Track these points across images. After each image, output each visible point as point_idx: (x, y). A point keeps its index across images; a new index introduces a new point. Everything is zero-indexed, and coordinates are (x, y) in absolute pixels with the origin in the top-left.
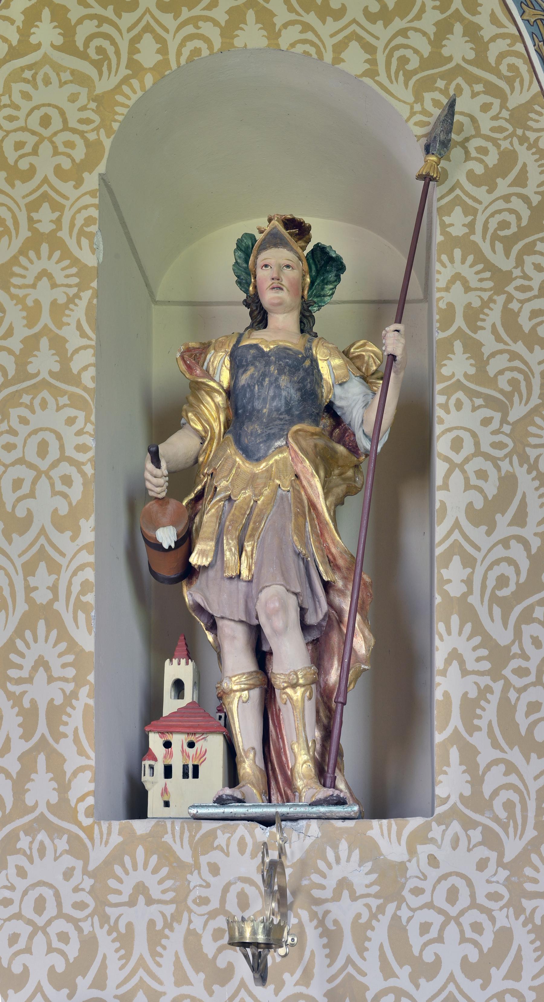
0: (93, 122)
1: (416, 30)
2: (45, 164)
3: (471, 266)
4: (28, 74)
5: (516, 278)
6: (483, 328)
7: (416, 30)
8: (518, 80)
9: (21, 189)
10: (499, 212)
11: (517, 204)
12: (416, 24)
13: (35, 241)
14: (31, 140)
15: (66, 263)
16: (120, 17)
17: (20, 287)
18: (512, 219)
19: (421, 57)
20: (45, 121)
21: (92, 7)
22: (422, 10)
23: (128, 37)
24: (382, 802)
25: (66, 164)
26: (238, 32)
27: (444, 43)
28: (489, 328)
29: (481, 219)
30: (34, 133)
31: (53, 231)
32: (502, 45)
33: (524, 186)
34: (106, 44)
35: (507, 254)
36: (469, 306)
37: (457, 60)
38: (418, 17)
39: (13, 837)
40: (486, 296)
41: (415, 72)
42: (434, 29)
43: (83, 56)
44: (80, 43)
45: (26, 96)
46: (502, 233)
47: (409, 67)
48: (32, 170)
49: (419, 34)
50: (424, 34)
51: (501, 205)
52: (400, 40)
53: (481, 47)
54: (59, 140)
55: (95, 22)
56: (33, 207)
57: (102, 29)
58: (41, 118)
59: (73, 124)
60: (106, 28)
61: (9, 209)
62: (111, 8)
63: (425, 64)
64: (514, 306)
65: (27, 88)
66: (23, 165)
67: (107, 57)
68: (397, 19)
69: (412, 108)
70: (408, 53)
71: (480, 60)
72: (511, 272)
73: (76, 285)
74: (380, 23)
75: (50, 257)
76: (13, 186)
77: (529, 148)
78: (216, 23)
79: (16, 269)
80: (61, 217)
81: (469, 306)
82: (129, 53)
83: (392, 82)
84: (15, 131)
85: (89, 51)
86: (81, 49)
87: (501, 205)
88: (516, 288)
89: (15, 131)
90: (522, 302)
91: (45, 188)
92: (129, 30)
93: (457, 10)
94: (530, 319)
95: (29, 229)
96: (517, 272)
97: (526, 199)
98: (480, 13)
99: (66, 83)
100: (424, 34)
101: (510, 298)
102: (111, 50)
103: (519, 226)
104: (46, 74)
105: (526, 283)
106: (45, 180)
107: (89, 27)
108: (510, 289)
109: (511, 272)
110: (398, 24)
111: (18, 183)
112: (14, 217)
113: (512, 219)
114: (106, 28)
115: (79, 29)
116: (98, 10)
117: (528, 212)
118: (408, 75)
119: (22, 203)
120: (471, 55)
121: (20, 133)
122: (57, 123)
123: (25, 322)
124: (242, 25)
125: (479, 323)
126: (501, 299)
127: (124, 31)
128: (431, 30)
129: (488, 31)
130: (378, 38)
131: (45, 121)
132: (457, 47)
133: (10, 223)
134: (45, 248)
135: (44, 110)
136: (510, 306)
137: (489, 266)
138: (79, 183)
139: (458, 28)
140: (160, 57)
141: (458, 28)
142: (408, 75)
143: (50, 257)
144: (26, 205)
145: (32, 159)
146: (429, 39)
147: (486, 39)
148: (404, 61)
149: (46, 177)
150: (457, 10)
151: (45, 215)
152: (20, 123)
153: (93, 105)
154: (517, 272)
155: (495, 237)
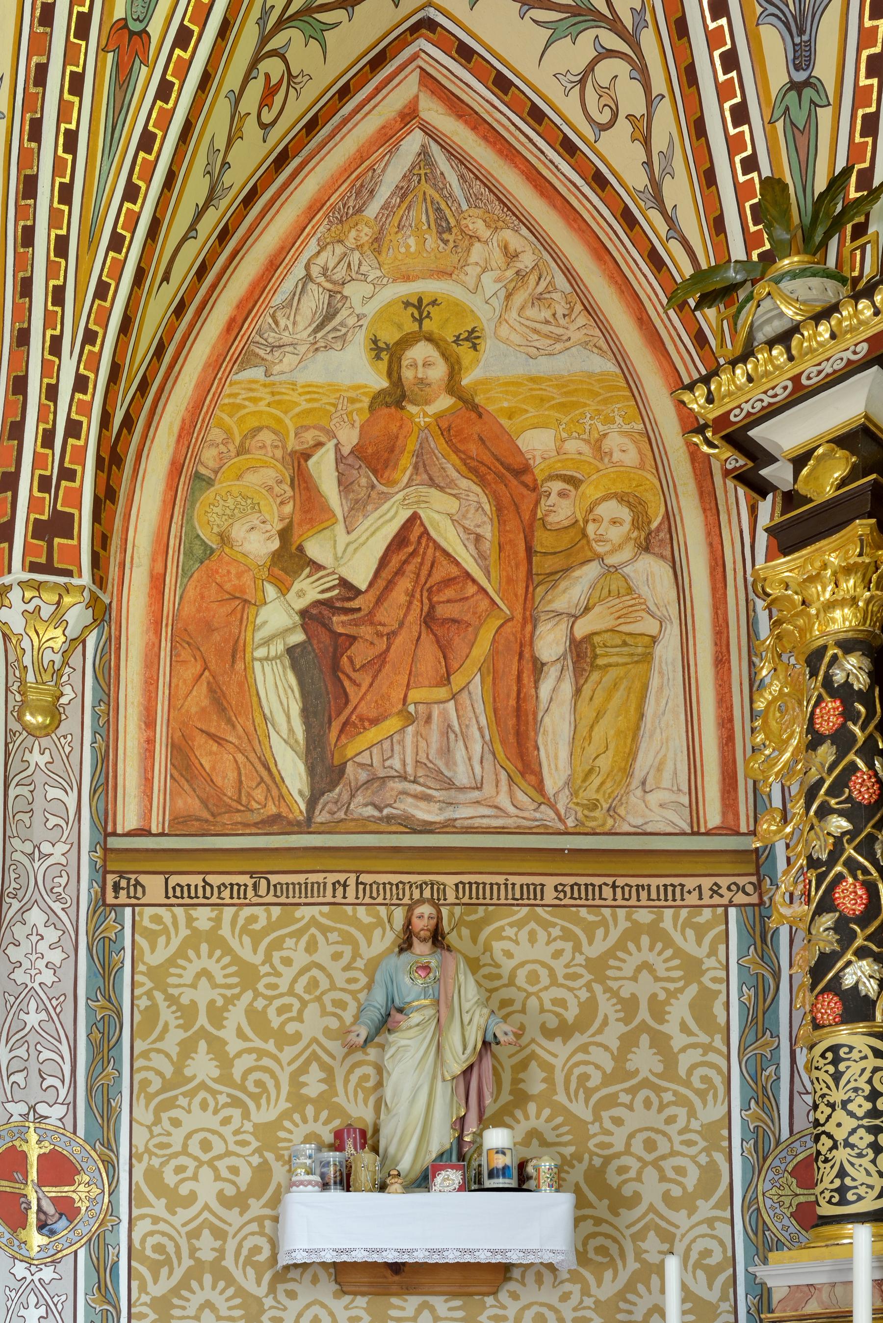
1: (159, 1051)
7: (159, 1051)
12: (158, 1045)
16: (281, 1050)
17: (616, 979)
19: (604, 1073)
21: (251, 1040)
22: (605, 1022)
23: (289, 1069)
25: (676, 1192)
26: (189, 1062)
27: (629, 1057)
29: (231, 1246)
32: (694, 1056)
34: (266, 1077)
37: (644, 1074)
38: (161, 1038)
39: (176, 1097)
41: (597, 1089)
42: (618, 1043)
43: (687, 1084)
44: (237, 1077)
47: (590, 1084)
49: (162, 1056)
50: (606, 1048)
53: (669, 1059)
55: (254, 1056)
57: (260, 1063)
60: (266, 1062)
62: (272, 1041)
63: (608, 1079)
68: (577, 1034)
69: (151, 1132)
70: (590, 1070)
71: (225, 1079)
74: (559, 1040)
83: (571, 1101)
85: (247, 1083)
91: (651, 1216)
92: (289, 1064)
93: (202, 1027)
98: (668, 1021)
100: (606, 1048)
102: (270, 1084)
107: (248, 1061)
110: (578, 1039)
114: (266, 1062)
115: (237, 1062)
116: (258, 1043)
118: (149, 1098)
120: (659, 1068)
124: (193, 1055)
127: (284, 1064)
128: (614, 1044)
129: (679, 1040)
130: (556, 1056)
132: (201, 1066)
138: (244, 1208)
139: (645, 1039)
140: (324, 1087)
141: (645, 1039)
142: (149, 1098)
144: (187, 1233)
146: (612, 1054)
147: (676, 1050)
148: (146, 1083)
149: (651, 1204)
150: (202, 1027)
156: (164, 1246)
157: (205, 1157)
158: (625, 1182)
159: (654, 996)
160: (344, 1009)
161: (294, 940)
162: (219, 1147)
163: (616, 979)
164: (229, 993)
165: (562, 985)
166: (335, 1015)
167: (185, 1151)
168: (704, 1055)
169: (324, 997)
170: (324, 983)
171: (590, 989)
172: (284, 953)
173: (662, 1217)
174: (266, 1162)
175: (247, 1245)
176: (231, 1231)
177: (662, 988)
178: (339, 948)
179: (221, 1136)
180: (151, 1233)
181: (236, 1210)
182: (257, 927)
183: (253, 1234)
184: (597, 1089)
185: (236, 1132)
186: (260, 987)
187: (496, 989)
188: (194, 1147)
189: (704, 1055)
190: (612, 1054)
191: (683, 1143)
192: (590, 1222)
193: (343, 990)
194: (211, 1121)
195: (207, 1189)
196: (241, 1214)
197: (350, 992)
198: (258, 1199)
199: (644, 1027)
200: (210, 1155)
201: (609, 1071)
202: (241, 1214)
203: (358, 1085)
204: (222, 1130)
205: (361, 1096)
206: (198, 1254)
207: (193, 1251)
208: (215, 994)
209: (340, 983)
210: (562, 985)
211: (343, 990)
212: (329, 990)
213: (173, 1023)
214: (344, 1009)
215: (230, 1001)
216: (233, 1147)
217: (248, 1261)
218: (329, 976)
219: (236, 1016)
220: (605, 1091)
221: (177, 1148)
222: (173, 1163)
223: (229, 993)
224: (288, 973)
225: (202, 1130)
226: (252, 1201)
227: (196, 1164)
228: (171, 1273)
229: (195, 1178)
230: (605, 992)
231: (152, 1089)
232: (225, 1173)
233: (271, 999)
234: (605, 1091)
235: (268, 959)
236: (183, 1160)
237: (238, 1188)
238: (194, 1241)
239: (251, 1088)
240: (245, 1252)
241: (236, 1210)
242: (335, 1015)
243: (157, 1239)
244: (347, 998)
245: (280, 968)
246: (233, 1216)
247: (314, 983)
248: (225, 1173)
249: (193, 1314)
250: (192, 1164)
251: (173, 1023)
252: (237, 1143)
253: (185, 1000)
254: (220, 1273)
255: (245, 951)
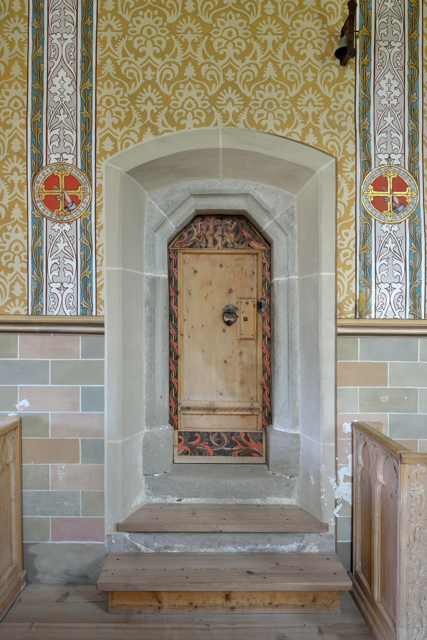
0: (249, 34)
2: (230, 51)
3: (235, 95)
4: (223, 14)
5: (253, 100)
6: (240, 122)
8: (173, 10)
9: (220, 63)
10: (246, 71)
11: (253, 68)
13: (227, 84)
14: (225, 42)
15: (239, 95)
17: (301, 106)
18: (251, 74)
19: (295, 6)
20: (230, 34)
22: (297, 123)
24: (102, 325)
28: (242, 122)
29: (158, 73)
30: (225, 39)
31: (233, 81)
33: (256, 60)
35: (249, 90)
36: (234, 112)
40: (241, 107)
45: (222, 24)
46: (247, 81)
47: (291, 10)
48: (224, 55)
51: (247, 68)
52: (126, 136)
54: (236, 41)
56: (225, 70)
58: (228, 32)
59: (241, 35)
61: (216, 72)
64: (252, 112)
65: (223, 20)
66: (221, 52)
67: (173, 8)
72: (250, 97)
73: (243, 105)
75: (232, 93)
76: (217, 62)
77: (257, 43)
78: (136, 132)
79: (219, 97)
80: (156, 73)
81: (234, 112)
82: (342, 9)
83: (284, 18)
84: (218, 38)
86: (323, 7)
87: (247, 68)
88: (253, 104)
89: (218, 38)
90: (255, 110)
94: (258, 118)
95: (224, 80)
96: (253, 98)
97: (257, 66)
99: (238, 18)
101: (250, 108)
103: (253, 77)
104: (230, 15)
105: (256, 102)
106: (230, 59)
108: (250, 104)
109: (250, 97)
111: (219, 60)
112: (218, 75)
113: (251, 74)
116: (332, 130)
117: (257, 72)
118: (290, 14)
119: (221, 69)
121: (220, 39)
122: (234, 35)
123: (222, 120)
125: (238, 120)
126: (166, 109)
131: (230, 34)
133: (216, 77)
134: (230, 89)
135: (229, 30)
136: (250, 112)
137: (242, 95)
138: (324, 61)
143: (232, 93)
144: (142, 68)
145: (225, 50)
148: (288, 8)
151: (230, 74)
152: (220, 35)
153: (249, 27)
154: (253, 98)
155: (244, 82)
156: (133, 74)
157: (149, 37)
158: (300, 49)
159: (314, 113)
160: (201, 117)
161: (183, 85)
162: (154, 33)
163: (301, 106)
164: (159, 107)
165: (281, 108)
166: (198, 118)
167: (141, 34)
168: (332, 136)
169: (194, 111)
170: (194, 106)
171: (291, 111)
172: (180, 91)
173: (314, 64)
174: (171, 39)
175: (165, 73)
176: (158, 67)
177: (317, 110)
178: (200, 91)
179: (155, 28)
180: (128, 68)
181: (160, 59)
182: (169, 79)
183: (166, 69)
184: (293, 12)
185: (161, 27)
186: (171, 105)
187: (257, 110)
188: (145, 32)
189: (332, 136)
190: (300, 136)
191: (321, 33)
192: (288, 65)
193: (201, 109)
194: (152, 22)
195: (149, 50)
196: (242, 62)
197: (203, 109)
198: (169, 54)
199: (310, 125)
200: (151, 36)
201: (297, 5)
202: (242, 62)
203: (206, 9)
204: (155, 25)
205: (207, 13)
206: (146, 77)
207: (144, 75)
208: (153, 107)
209: (200, 106)
210: (281, 108)
211: (201, 109)
212: (196, 109)
213: (138, 119)
214: (201, 117)
215: (159, 110)
216: (159, 33)
217: (165, 81)
218: (196, 102)
219: (162, 117)
220: (295, 13)
221: (139, 32)
222: (137, 39)
223: (159, 107)
224: (181, 99)
225: (148, 25)
226: (246, 57)
227: (146, 39)
228: (136, 85)
229: (145, 45)
230: (296, 111)
231: (131, 7)
232: (156, 44)
233: (175, 110)
234: (295, 13)
235: (174, 93)
236: (140, 38)
237: (161, 50)
238: (145, 72)
239: (328, 11)
240: (163, 77)
241: (160, 59)
242: (198, 118)
243: (131, 70)
244: (203, 112)
245: (178, 97)
246: (159, 61)
247: (190, 105)
248: (156, 44)
249: (144, 102)
250: (144, 39)
251: (138, 119)
252: (161, 31)
253: (142, 110)
254: (155, 86)
255: (165, 90)
